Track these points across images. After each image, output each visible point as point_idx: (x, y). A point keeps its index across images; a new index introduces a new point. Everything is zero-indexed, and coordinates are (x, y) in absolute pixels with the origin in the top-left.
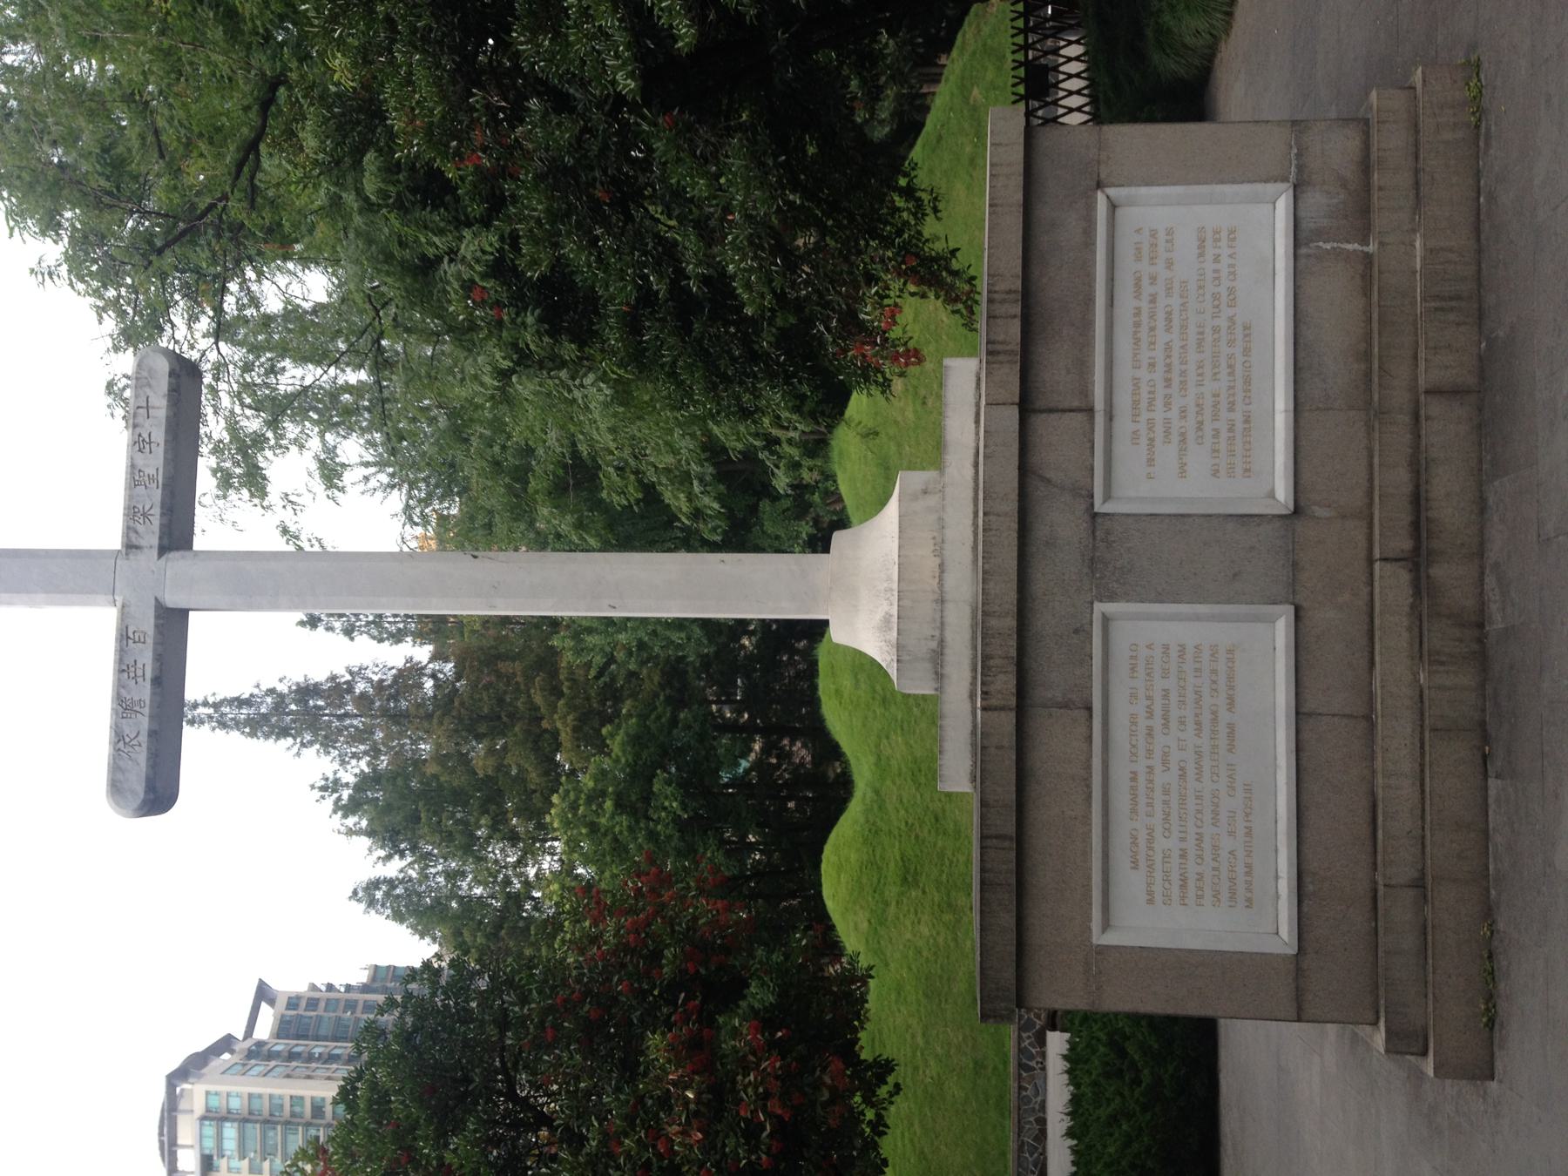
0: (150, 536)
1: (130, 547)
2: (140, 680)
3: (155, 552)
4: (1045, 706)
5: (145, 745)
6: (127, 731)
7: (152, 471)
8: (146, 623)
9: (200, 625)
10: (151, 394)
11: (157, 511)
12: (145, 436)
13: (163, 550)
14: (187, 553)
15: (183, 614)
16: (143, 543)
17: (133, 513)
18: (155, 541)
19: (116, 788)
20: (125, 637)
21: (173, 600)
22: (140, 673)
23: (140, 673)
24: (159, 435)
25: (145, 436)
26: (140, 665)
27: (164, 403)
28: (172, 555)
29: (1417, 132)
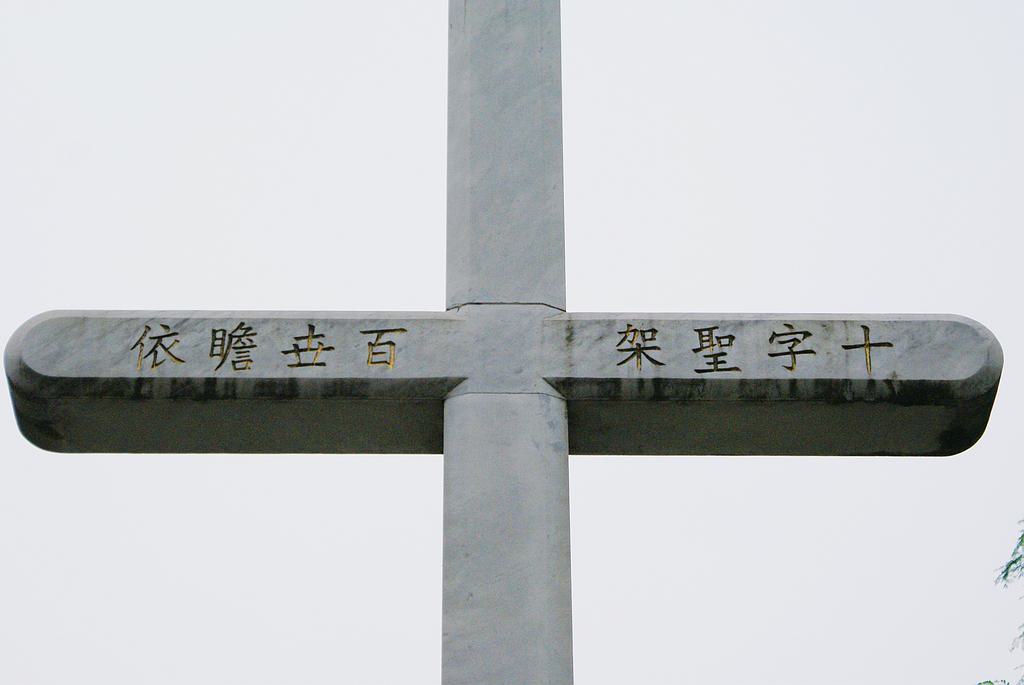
0: (595, 363)
1: (571, 330)
2: (293, 358)
3: (561, 373)
4: (581, 327)
5: (154, 373)
6: (184, 339)
7: (732, 357)
8: (404, 366)
9: (416, 476)
10: (896, 350)
11: (648, 372)
12: (807, 344)
13: (564, 385)
14: (561, 433)
15: (433, 443)
16: (577, 351)
17: (640, 337)
18: (581, 372)
19: (73, 326)
20: (380, 332)
21: (458, 412)
22: (306, 357)
23: (306, 357)
24: (808, 369)
25: (807, 344)
26: (322, 356)
27: (880, 374)
28: (557, 407)
29: (263, 322)
